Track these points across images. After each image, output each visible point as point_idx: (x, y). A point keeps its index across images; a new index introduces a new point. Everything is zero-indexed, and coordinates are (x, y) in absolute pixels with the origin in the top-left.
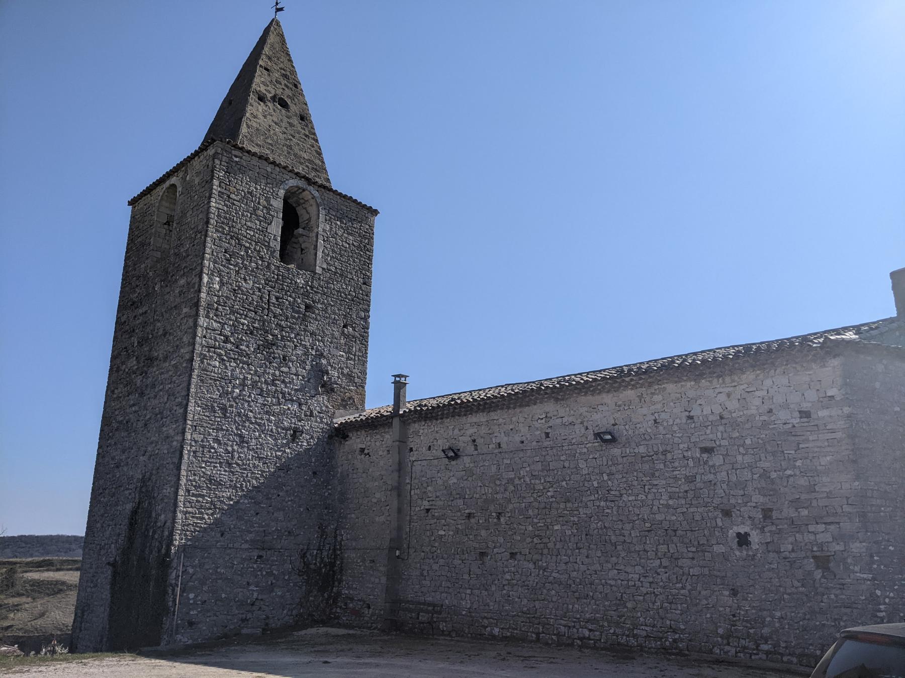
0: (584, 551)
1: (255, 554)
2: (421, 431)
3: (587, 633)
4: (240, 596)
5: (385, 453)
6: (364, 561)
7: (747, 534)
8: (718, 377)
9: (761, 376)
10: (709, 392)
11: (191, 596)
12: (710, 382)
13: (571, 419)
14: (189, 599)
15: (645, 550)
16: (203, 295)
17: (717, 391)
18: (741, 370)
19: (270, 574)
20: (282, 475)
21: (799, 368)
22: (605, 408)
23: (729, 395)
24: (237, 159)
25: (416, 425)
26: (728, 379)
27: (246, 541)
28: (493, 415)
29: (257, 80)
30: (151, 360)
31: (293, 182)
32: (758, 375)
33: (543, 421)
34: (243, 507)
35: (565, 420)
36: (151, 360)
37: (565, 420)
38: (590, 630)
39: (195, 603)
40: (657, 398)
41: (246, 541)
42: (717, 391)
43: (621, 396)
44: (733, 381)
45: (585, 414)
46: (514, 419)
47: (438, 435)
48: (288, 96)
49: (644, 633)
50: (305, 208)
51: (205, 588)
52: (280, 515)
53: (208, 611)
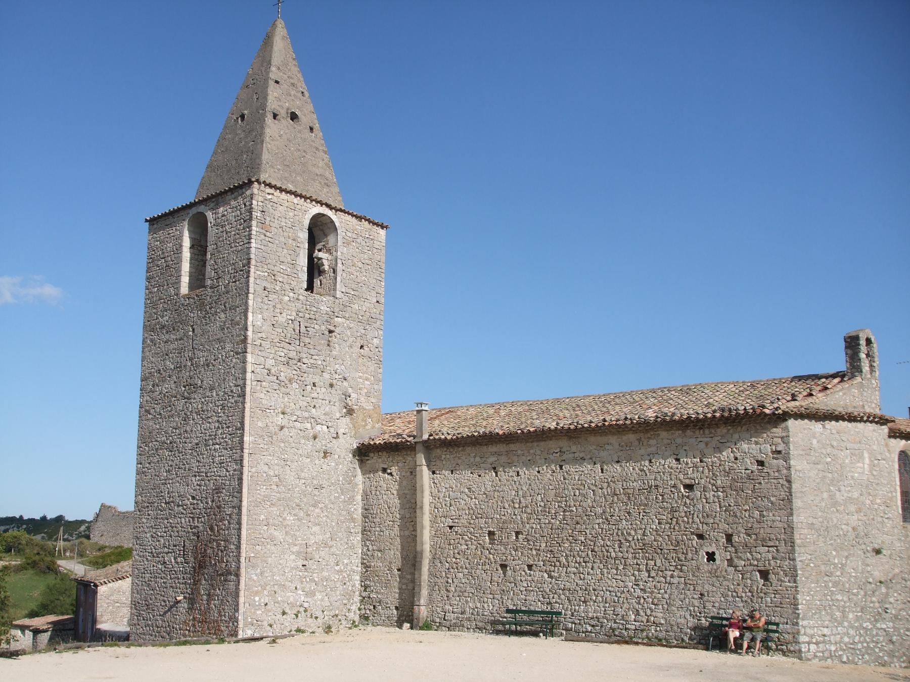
0: (590, 565)
1: (300, 563)
2: (444, 456)
3: (589, 628)
4: (291, 599)
5: (408, 474)
6: (390, 569)
7: (713, 553)
8: (700, 429)
9: (731, 431)
10: (693, 441)
11: (257, 599)
12: (694, 432)
13: (582, 455)
14: (254, 600)
15: (637, 564)
16: (250, 333)
17: (699, 440)
18: (716, 425)
19: (312, 580)
20: (317, 493)
21: (758, 427)
22: (610, 447)
23: (707, 444)
24: (270, 197)
25: (438, 451)
26: (707, 431)
27: (293, 553)
28: (512, 447)
29: (270, 98)
30: (192, 387)
31: (317, 209)
32: (729, 430)
33: (558, 455)
34: (289, 523)
35: (576, 455)
36: (192, 387)
37: (576, 455)
38: (593, 626)
39: (260, 605)
40: (653, 442)
41: (293, 553)
42: (699, 440)
43: (624, 438)
44: (711, 433)
45: (594, 451)
46: (532, 451)
47: (459, 462)
48: (299, 108)
49: (633, 627)
50: (322, 230)
51: (266, 592)
52: (316, 529)
53: (269, 611)
